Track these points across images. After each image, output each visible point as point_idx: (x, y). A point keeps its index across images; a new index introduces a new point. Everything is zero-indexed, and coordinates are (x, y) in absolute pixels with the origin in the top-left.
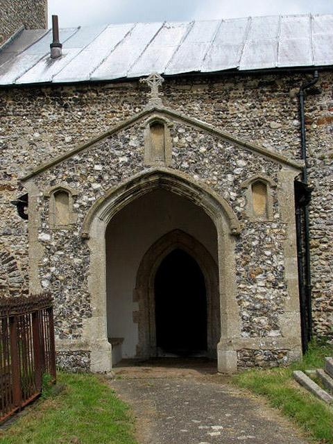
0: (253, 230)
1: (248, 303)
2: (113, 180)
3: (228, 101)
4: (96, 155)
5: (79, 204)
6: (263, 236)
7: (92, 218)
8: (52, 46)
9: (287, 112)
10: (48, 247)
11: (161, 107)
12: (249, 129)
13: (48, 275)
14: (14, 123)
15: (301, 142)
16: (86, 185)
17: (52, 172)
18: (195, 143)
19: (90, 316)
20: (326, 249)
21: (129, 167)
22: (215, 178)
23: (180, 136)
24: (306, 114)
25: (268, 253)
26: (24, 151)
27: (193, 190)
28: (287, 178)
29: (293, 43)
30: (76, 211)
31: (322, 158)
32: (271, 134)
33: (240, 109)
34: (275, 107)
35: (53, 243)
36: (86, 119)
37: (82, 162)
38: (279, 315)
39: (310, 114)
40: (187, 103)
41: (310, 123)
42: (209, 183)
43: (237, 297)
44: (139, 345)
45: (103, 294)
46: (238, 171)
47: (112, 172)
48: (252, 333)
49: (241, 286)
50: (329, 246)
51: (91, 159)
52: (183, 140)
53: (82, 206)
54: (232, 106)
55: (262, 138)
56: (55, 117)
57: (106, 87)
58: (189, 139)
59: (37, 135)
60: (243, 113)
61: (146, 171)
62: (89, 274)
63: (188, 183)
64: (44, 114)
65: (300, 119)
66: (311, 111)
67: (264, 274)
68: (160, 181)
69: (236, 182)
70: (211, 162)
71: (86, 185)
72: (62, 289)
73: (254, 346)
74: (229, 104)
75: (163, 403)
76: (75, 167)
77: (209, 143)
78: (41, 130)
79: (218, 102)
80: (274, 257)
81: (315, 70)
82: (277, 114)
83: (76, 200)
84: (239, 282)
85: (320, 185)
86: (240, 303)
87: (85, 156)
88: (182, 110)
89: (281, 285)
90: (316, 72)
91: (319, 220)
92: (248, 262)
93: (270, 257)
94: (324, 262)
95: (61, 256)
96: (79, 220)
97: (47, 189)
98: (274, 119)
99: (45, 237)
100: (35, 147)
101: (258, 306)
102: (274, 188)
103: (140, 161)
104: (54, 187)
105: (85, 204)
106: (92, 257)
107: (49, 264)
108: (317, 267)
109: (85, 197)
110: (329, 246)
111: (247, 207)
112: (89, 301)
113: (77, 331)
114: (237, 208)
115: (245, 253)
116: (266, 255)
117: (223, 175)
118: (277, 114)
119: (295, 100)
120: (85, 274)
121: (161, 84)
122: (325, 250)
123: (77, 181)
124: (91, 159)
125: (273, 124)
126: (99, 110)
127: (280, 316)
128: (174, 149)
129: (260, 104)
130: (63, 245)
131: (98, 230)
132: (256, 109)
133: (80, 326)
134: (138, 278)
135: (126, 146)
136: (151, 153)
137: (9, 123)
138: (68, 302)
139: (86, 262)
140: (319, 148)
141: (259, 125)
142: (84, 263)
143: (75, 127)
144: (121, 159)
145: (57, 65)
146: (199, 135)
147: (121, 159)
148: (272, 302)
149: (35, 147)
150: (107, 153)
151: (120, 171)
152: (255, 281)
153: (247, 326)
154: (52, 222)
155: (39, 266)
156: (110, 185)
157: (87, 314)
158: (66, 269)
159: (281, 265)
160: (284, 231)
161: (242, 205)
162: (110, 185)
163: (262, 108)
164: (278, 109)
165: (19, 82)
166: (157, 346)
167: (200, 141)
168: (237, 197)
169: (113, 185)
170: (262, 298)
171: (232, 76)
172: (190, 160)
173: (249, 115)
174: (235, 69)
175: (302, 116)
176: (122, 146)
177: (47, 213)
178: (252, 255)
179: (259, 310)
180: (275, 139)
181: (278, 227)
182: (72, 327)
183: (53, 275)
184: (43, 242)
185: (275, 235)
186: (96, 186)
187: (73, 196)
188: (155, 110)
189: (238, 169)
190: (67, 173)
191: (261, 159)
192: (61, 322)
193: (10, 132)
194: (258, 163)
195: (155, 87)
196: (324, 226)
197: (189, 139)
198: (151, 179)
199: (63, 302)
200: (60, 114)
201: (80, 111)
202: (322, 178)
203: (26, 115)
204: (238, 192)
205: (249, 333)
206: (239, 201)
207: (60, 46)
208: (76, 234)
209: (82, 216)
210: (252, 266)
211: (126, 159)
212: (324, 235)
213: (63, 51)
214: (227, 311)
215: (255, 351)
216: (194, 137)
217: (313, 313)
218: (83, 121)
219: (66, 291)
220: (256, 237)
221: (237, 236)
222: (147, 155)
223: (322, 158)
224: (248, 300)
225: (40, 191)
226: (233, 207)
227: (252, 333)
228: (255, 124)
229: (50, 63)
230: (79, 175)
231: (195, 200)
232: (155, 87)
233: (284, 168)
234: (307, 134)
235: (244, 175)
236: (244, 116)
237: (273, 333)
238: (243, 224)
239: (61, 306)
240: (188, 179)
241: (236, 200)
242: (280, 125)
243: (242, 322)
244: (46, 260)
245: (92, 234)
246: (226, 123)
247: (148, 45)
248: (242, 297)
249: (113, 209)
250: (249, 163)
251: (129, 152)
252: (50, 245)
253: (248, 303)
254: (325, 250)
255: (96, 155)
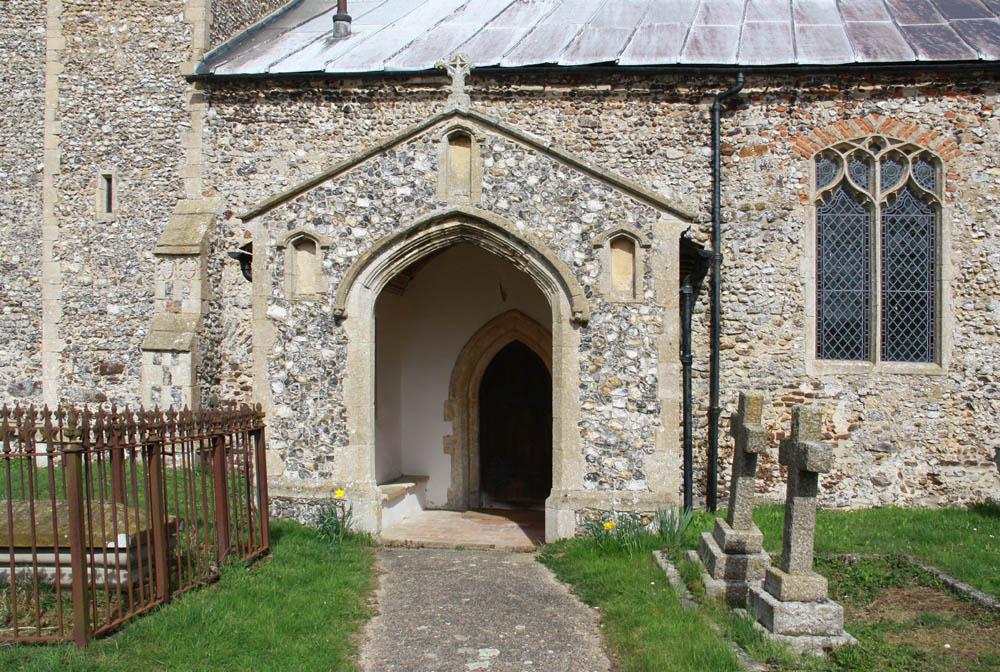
0: (610, 316)
1: (596, 435)
2: (387, 223)
3: (600, 112)
4: (361, 182)
5: (332, 260)
6: (625, 326)
7: (351, 284)
8: (335, 19)
9: (693, 134)
10: (282, 328)
11: (464, 109)
12: (632, 157)
13: (283, 374)
14: (266, 133)
15: (714, 182)
16: (344, 230)
17: (290, 207)
18: (520, 169)
19: (346, 443)
20: (746, 352)
21: (412, 204)
22: (551, 228)
23: (496, 156)
24: (723, 139)
25: (632, 354)
26: (280, 178)
27: (513, 245)
28: (667, 233)
29: (712, 31)
30: (326, 272)
31: (745, 209)
32: (667, 168)
33: (619, 120)
34: (676, 126)
35: (291, 323)
36: (376, 131)
37: (338, 193)
38: (646, 456)
39: (730, 139)
40: (537, 112)
41: (730, 154)
42: (540, 235)
43: (580, 424)
44: (452, 490)
45: (368, 408)
46: (588, 218)
47: (386, 210)
48: (601, 483)
49: (587, 406)
50: (751, 347)
51: (352, 189)
52: (501, 163)
53: (335, 264)
54: (606, 120)
55: (653, 173)
56: (330, 127)
57: (409, 82)
58: (511, 162)
59: (301, 153)
60: (624, 132)
61: (439, 211)
62: (345, 375)
63: (507, 234)
64: (312, 121)
65: (713, 146)
66: (730, 134)
67: (624, 387)
68: (462, 230)
69: (584, 235)
70: (545, 201)
71: (344, 230)
72: (303, 397)
73: (601, 505)
74: (602, 117)
75: (277, 660)
76: (326, 201)
77: (544, 170)
78: (308, 145)
79: (586, 113)
80: (642, 360)
81: (739, 72)
82: (678, 137)
83: (327, 254)
84: (583, 399)
85: (741, 251)
86: (584, 432)
87: (342, 183)
88: (528, 123)
89: (651, 407)
90: (741, 75)
91: (736, 305)
92: (599, 367)
93: (636, 362)
94: (741, 372)
95: (302, 344)
96: (331, 287)
97: (282, 235)
98: (671, 144)
99: (278, 312)
100: (297, 172)
101: (612, 440)
102: (647, 247)
103: (430, 194)
104: (292, 232)
105: (341, 261)
106: (350, 349)
107: (283, 357)
108: (730, 379)
109: (341, 251)
110: (751, 347)
111: (601, 277)
112: (345, 419)
113: (327, 467)
114: (586, 279)
115: (595, 353)
116: (628, 358)
117: (564, 224)
118: (678, 137)
119: (707, 116)
120: (338, 375)
121: (469, 72)
122: (745, 353)
123: (328, 223)
124: (352, 189)
125: (672, 152)
126: (398, 118)
127: (647, 459)
128: (486, 178)
129: (652, 120)
130: (306, 327)
131: (361, 304)
132: (645, 127)
133: (330, 458)
134: (452, 386)
135: (408, 169)
136: (452, 180)
137: (260, 133)
138: (312, 419)
139: (341, 357)
140: (741, 193)
141: (650, 152)
142: (338, 357)
143: (360, 143)
144: (400, 191)
145: (341, 46)
146: (527, 155)
147: (400, 191)
148: (636, 434)
149: (297, 172)
150: (377, 180)
151: (397, 209)
152: (609, 399)
153: (594, 471)
154: (288, 289)
155: (269, 359)
156: (382, 232)
157: (341, 440)
158: (309, 366)
159: (653, 375)
160: (659, 320)
161: (593, 274)
162: (382, 232)
163: (654, 125)
164: (679, 129)
165: (274, 70)
166: (480, 492)
167: (529, 167)
168: (586, 260)
169: (387, 231)
170: (620, 427)
171: (607, 73)
172: (512, 197)
173: (633, 136)
174: (612, 64)
175: (717, 142)
176: (402, 169)
177: (280, 274)
178: (606, 356)
179: (614, 446)
180: (673, 175)
181: (650, 313)
182: (319, 459)
183: (290, 375)
184: (275, 320)
185: (646, 325)
186: (359, 232)
187: (323, 248)
188: (456, 113)
189: (588, 215)
190: (313, 209)
191: (628, 200)
192: (302, 451)
193: (260, 147)
194: (623, 206)
195: (458, 75)
196: (745, 316)
197: (511, 162)
198: (446, 225)
199: (305, 419)
200: (338, 121)
201: (369, 118)
202: (744, 239)
203: (286, 122)
204: (588, 252)
205: (597, 483)
206: (589, 266)
207: (349, 20)
208: (326, 309)
209: (336, 280)
210: (606, 375)
211: (407, 191)
212: (744, 330)
213: (353, 27)
214: (563, 445)
215: (605, 512)
216: (519, 159)
217: (719, 450)
218: (373, 134)
219: (310, 401)
220: (614, 328)
221: (581, 324)
222: (440, 187)
223: (745, 209)
224: (597, 430)
225: (272, 237)
226: (579, 276)
227: (601, 483)
228: (642, 151)
229: (330, 43)
230: (332, 214)
231: (518, 264)
232: (458, 75)
233: (664, 215)
234: (724, 169)
235: (599, 225)
236: (626, 137)
237: (634, 485)
238: (594, 306)
239: (302, 425)
240: (506, 228)
241: (584, 265)
242: (682, 154)
243: (586, 464)
244: (279, 349)
245: (351, 310)
246: (596, 145)
247: (487, 24)
248: (587, 425)
249: (387, 271)
250: (607, 206)
251: (412, 179)
252: (285, 326)
253: (596, 435)
254: (745, 353)
255: (361, 182)
